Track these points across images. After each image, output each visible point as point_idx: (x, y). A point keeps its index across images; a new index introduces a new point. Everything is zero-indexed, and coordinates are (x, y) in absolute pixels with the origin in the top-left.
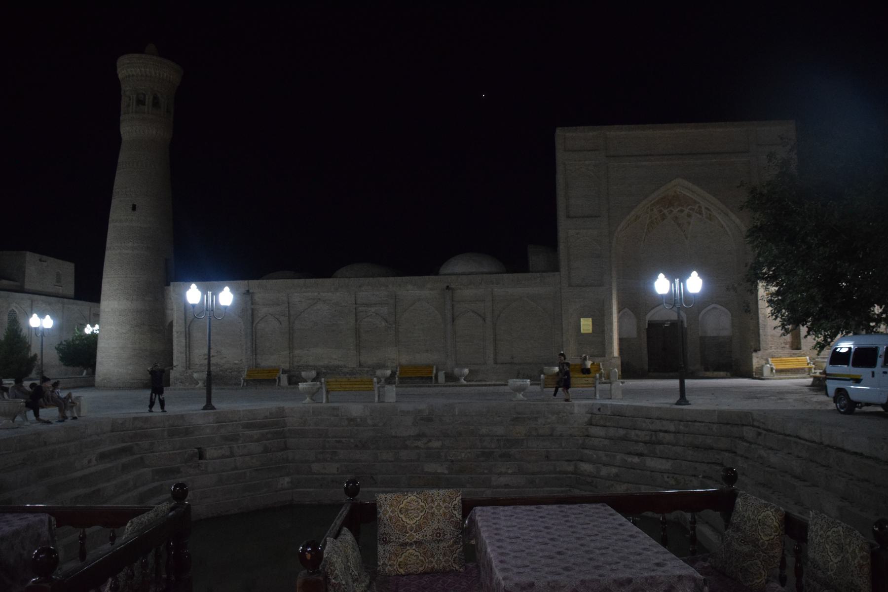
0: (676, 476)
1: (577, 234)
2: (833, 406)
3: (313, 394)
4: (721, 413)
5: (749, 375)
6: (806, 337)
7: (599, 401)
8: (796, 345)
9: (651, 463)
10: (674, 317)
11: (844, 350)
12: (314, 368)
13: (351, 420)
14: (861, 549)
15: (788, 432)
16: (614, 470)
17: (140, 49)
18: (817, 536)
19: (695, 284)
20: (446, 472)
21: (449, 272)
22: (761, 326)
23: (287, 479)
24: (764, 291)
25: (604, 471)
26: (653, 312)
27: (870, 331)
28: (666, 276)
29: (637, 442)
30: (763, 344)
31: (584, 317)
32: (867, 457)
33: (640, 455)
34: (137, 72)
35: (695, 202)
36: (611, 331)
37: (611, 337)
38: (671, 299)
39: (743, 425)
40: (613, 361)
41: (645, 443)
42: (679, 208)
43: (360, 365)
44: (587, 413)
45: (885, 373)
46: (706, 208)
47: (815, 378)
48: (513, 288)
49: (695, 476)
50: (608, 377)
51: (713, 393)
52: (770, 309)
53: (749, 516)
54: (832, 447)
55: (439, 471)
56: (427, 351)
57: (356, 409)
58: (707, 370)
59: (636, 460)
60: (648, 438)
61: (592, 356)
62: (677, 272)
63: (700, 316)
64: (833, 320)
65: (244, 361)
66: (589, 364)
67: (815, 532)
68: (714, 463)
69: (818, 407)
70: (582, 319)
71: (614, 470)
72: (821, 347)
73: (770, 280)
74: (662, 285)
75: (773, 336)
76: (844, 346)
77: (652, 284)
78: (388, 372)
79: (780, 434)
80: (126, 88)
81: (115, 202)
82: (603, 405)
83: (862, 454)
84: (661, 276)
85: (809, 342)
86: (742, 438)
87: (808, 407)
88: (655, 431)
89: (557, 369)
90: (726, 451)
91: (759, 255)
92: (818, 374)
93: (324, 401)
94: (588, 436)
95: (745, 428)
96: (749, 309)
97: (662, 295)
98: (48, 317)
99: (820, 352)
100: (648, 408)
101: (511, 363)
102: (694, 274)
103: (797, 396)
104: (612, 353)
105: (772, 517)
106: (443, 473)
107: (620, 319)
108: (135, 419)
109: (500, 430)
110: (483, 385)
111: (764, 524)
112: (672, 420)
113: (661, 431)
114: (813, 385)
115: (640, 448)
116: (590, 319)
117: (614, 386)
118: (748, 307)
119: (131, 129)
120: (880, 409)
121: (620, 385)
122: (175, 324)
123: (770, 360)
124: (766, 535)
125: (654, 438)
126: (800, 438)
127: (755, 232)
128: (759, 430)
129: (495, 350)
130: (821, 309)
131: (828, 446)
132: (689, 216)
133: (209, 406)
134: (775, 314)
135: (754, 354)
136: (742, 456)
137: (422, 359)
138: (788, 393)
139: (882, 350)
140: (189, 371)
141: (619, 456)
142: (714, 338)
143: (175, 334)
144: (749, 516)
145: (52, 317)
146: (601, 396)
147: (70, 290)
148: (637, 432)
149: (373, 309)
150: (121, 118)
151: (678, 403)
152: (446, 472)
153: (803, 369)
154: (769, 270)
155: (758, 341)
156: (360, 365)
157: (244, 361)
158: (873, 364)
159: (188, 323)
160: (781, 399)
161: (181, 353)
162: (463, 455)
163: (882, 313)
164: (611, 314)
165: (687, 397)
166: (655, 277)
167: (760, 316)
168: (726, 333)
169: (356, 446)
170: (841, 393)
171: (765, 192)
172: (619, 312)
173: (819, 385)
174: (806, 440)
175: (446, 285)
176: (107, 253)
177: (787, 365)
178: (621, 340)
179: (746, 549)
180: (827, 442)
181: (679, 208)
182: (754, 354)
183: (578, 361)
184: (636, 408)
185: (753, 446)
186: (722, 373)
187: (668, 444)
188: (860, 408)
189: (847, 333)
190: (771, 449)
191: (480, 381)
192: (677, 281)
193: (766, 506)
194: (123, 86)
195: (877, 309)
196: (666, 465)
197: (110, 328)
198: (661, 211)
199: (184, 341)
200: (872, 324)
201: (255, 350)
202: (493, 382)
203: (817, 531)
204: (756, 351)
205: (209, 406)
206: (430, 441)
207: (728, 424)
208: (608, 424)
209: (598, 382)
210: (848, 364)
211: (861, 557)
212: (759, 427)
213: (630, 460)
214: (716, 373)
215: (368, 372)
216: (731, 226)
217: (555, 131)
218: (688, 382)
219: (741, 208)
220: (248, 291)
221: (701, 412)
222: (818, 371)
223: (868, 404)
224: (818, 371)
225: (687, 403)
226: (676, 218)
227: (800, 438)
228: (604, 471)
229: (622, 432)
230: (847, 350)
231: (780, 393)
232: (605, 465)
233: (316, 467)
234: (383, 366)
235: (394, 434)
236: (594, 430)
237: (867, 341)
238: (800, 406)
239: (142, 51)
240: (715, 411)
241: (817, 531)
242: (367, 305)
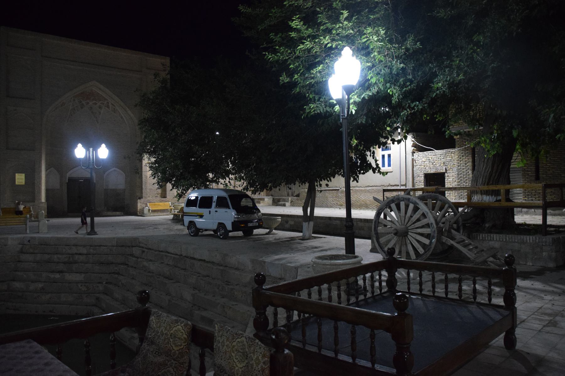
0: (86, 284)
2: (186, 231)
4: (119, 239)
5: (136, 214)
6: (171, 190)
7: (29, 235)
8: (164, 195)
9: (69, 277)
10: (88, 176)
11: (193, 198)
14: (264, 356)
15: (161, 250)
18: (223, 346)
19: (103, 152)
24: (147, 161)
26: (71, 171)
27: (206, 187)
28: (84, 146)
29: (58, 263)
32: (208, 262)
33: (61, 272)
36: (40, 184)
38: (86, 162)
39: (133, 246)
40: (41, 205)
41: (64, 263)
44: (20, 244)
45: (216, 211)
47: (174, 215)
49: (99, 283)
50: (37, 217)
51: (112, 226)
52: (151, 172)
53: (162, 331)
54: (188, 257)
58: (108, 210)
59: (57, 276)
61: (24, 202)
62: (91, 144)
63: (105, 175)
64: (188, 180)
66: (21, 207)
67: (222, 342)
68: (113, 273)
69: (178, 233)
70: (17, 174)
71: (40, 285)
72: (180, 196)
73: (151, 153)
74: (80, 152)
75: (151, 189)
76: (193, 196)
77: (73, 152)
79: (156, 251)
82: (32, 238)
83: (204, 260)
84: (80, 146)
85: (172, 192)
86: (132, 255)
87: (172, 233)
88: (73, 254)
90: (122, 264)
91: (145, 137)
92: (176, 213)
94: (19, 261)
95: (134, 248)
96: (138, 171)
97: (80, 159)
99: (179, 199)
100: (68, 238)
102: (103, 146)
103: (166, 226)
104: (41, 199)
105: (181, 330)
107: (47, 176)
111: (175, 337)
112: (84, 246)
113: (76, 254)
114: (173, 219)
116: (24, 175)
117: (41, 223)
118: (138, 170)
120: (212, 233)
121: (45, 222)
124: (177, 346)
125: (71, 259)
126: (169, 253)
127: (143, 122)
128: (144, 249)
130: (181, 173)
131: (185, 257)
132: (100, 107)
134: (154, 175)
135: (139, 201)
136: (132, 267)
138: (160, 224)
139: (215, 199)
144: (162, 331)
146: (30, 231)
148: (60, 256)
151: (89, 234)
153: (167, 210)
154: (151, 147)
158: (209, 206)
160: (156, 228)
163: (214, 177)
164: (40, 172)
165: (96, 230)
167: (143, 176)
170: (192, 223)
171: (151, 97)
172: (46, 170)
173: (178, 219)
174: (172, 254)
177: (160, 206)
178: (47, 190)
179: (160, 359)
180: (184, 255)
181: (94, 102)
182: (139, 201)
184: (58, 239)
185: (139, 260)
186: (118, 213)
187: (81, 262)
188: (202, 232)
189: (194, 188)
190: (151, 261)
192: (91, 149)
193: (177, 321)
195: (211, 175)
200: (208, 183)
203: (223, 342)
204: (140, 198)
207: (123, 246)
209: (28, 221)
210: (196, 207)
211: (264, 363)
212: (143, 247)
213: (53, 276)
214: (114, 213)
216: (129, 117)
217: (26, 182)
218: (96, 219)
219: (136, 106)
221: (105, 239)
222: (176, 211)
223: (206, 230)
224: (176, 211)
225: (95, 233)
226: (91, 108)
227: (169, 253)
229: (47, 257)
230: (194, 198)
231: (155, 225)
232: (32, 282)
236: (24, 257)
237: (206, 193)
238: (167, 233)
240: (114, 238)
241: (223, 342)
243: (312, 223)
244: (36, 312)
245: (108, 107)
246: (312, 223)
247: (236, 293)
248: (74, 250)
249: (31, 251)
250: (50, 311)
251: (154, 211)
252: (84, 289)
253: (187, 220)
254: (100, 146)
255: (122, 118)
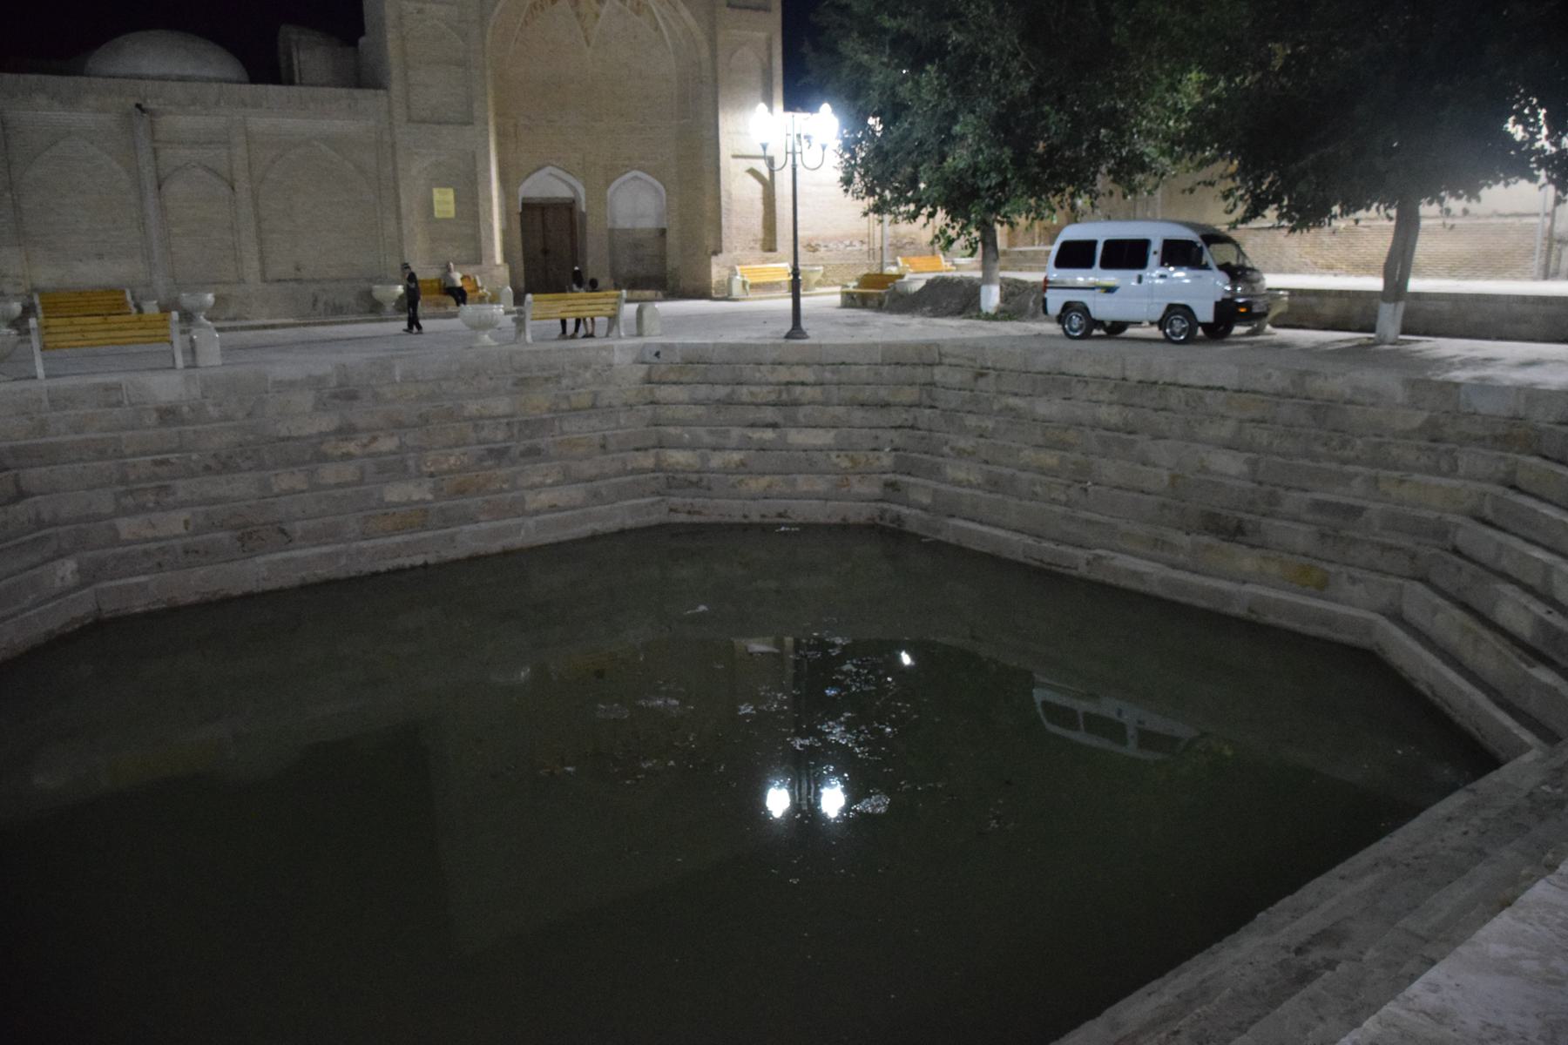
1: (420, 11)
4: (888, 347)
5: (703, 293)
9: (796, 437)
13: (168, 415)
16: (737, 456)
20: (429, 497)
25: (716, 460)
33: (774, 426)
36: (491, 215)
37: (491, 226)
40: (495, 272)
48: (299, 119)
55: (415, 497)
56: (100, 256)
59: (769, 434)
60: (773, 397)
66: (457, 277)
70: (435, 191)
71: (737, 456)
82: (664, 346)
89: (400, 289)
93: (40, 372)
101: (296, 280)
104: (493, 257)
106: (423, 501)
109: (502, 405)
115: (769, 414)
129: (261, 251)
141: (736, 432)
142: (626, 231)
148: (753, 389)
155: (719, 239)
162: (452, 460)
164: (489, 182)
165: (804, 325)
168: (649, 223)
169: (208, 468)
175: (133, 101)
191: (234, 319)
196: (824, 438)
204: (715, 253)
206: (375, 439)
208: (684, 379)
228: (716, 460)
229: (721, 392)
232: (714, 449)
233: (127, 527)
236: (663, 392)
243: (1401, 306)
246: (1401, 306)
247: (1395, 452)
248: (783, 374)
249: (672, 377)
250: (780, 515)
251: (755, 286)
252: (845, 463)
253: (1055, 300)
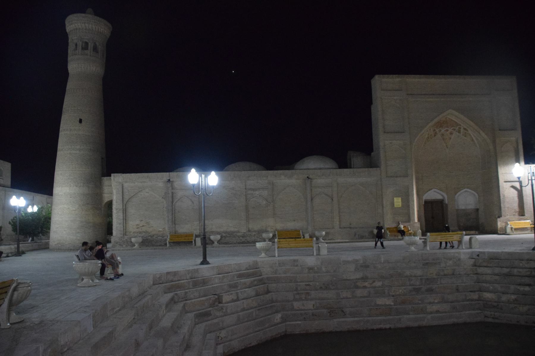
1: (391, 143)
3: (267, 250)
5: (495, 232)
12: (218, 233)
13: (311, 269)
17: (82, 11)
20: (392, 304)
21: (304, 168)
22: (502, 201)
23: (280, 315)
25: (504, 298)
30: (503, 213)
31: (396, 197)
34: (82, 27)
35: (457, 124)
38: (196, 188)
42: (446, 129)
43: (249, 231)
46: (465, 129)
48: (355, 178)
55: (387, 303)
56: (294, 221)
57: (310, 261)
60: (528, 273)
61: (403, 222)
65: (167, 229)
70: (395, 198)
78: (271, 235)
80: (73, 39)
81: (65, 118)
82: (481, 252)
84: (193, 171)
98: (22, 198)
104: (414, 220)
108: (168, 273)
109: (419, 272)
110: (333, 243)
119: (75, 66)
122: (114, 203)
123: (509, 222)
132: (451, 134)
133: (205, 262)
137: (291, 225)
140: (126, 237)
141: (512, 287)
142: (464, 210)
143: (114, 211)
145: (25, 199)
147: (8, 182)
149: (257, 193)
150: (69, 59)
152: (392, 304)
153: (526, 228)
156: (249, 231)
157: (167, 229)
159: (125, 202)
161: (120, 224)
162: (401, 291)
165: (208, 259)
166: (11, 197)
175: (306, 176)
176: (59, 153)
181: (446, 129)
182: (498, 219)
183: (394, 225)
194: (70, 37)
197: (66, 206)
198: (435, 130)
199: (122, 215)
201: (174, 222)
202: (339, 241)
204: (499, 217)
205: (205, 262)
206: (374, 282)
215: (255, 235)
217: (402, 205)
220: (169, 180)
228: (504, 298)
229: (506, 270)
233: (296, 305)
234: (266, 231)
235: (345, 278)
236: (480, 270)
239: (84, 12)
242: (254, 190)
244: (518, 322)
245: (459, 132)
249: (485, 264)
251: (516, 229)
254: (190, 171)
255: (473, 140)
